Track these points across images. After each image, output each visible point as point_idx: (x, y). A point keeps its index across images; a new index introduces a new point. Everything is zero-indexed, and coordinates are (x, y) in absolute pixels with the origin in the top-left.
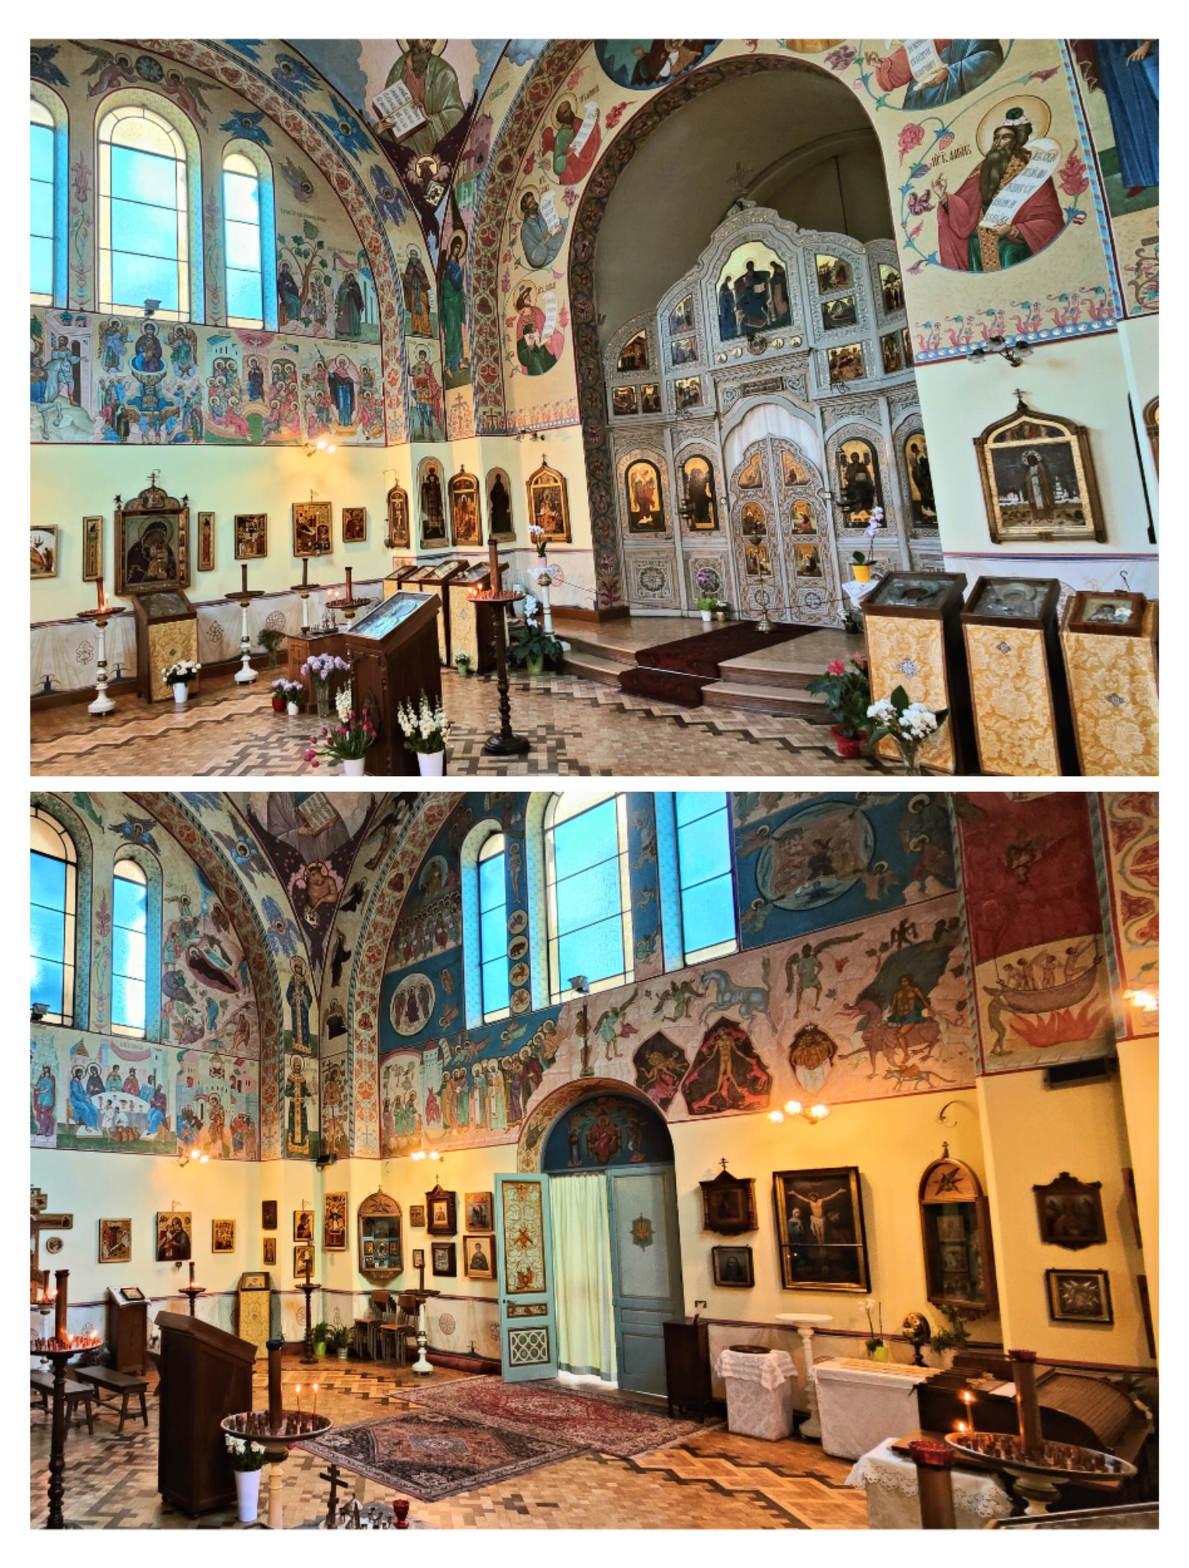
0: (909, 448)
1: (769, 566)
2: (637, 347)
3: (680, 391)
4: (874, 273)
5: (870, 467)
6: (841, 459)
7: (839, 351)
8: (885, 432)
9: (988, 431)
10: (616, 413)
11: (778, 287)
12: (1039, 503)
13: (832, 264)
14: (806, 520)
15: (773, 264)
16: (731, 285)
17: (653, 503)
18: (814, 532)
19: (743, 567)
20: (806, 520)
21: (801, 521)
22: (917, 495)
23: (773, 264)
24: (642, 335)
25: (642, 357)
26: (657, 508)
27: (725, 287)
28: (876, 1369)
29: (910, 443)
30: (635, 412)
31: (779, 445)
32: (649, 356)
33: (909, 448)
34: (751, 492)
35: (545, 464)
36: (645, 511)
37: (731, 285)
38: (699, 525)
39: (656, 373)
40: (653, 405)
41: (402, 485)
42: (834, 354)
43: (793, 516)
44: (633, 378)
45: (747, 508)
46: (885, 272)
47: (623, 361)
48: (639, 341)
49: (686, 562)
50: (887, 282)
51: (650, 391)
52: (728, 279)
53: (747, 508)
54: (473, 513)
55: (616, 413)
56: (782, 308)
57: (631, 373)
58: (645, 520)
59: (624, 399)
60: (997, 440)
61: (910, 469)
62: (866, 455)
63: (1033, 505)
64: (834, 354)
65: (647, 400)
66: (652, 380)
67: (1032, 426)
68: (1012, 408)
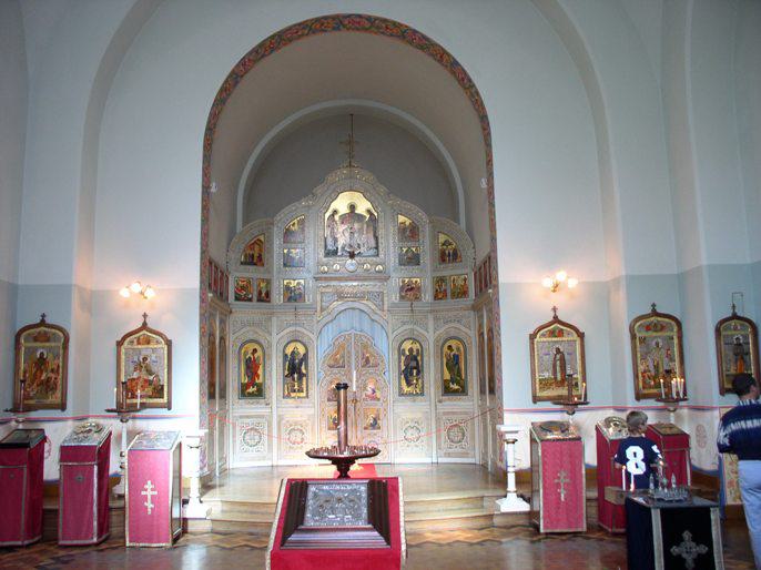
0: (446, 346)
3: (287, 288)
4: (435, 238)
5: (419, 358)
6: (401, 352)
7: (407, 280)
10: (237, 299)
12: (559, 377)
13: (407, 223)
14: (374, 392)
15: (369, 211)
18: (379, 399)
20: (374, 392)
22: (447, 376)
23: (369, 211)
25: (260, 257)
28: (719, 557)
29: (448, 344)
30: (250, 300)
32: (265, 256)
33: (446, 346)
34: (336, 370)
35: (145, 324)
36: (252, 383)
38: (293, 395)
39: (269, 271)
40: (265, 297)
42: (403, 282)
43: (365, 389)
44: (252, 273)
46: (442, 238)
47: (246, 256)
50: (443, 245)
51: (263, 285)
52: (335, 212)
55: (237, 299)
57: (252, 268)
58: (251, 390)
59: (243, 288)
60: (543, 335)
62: (418, 350)
63: (556, 378)
64: (403, 282)
65: (260, 293)
66: (266, 276)
67: (46, 333)
68: (551, 319)
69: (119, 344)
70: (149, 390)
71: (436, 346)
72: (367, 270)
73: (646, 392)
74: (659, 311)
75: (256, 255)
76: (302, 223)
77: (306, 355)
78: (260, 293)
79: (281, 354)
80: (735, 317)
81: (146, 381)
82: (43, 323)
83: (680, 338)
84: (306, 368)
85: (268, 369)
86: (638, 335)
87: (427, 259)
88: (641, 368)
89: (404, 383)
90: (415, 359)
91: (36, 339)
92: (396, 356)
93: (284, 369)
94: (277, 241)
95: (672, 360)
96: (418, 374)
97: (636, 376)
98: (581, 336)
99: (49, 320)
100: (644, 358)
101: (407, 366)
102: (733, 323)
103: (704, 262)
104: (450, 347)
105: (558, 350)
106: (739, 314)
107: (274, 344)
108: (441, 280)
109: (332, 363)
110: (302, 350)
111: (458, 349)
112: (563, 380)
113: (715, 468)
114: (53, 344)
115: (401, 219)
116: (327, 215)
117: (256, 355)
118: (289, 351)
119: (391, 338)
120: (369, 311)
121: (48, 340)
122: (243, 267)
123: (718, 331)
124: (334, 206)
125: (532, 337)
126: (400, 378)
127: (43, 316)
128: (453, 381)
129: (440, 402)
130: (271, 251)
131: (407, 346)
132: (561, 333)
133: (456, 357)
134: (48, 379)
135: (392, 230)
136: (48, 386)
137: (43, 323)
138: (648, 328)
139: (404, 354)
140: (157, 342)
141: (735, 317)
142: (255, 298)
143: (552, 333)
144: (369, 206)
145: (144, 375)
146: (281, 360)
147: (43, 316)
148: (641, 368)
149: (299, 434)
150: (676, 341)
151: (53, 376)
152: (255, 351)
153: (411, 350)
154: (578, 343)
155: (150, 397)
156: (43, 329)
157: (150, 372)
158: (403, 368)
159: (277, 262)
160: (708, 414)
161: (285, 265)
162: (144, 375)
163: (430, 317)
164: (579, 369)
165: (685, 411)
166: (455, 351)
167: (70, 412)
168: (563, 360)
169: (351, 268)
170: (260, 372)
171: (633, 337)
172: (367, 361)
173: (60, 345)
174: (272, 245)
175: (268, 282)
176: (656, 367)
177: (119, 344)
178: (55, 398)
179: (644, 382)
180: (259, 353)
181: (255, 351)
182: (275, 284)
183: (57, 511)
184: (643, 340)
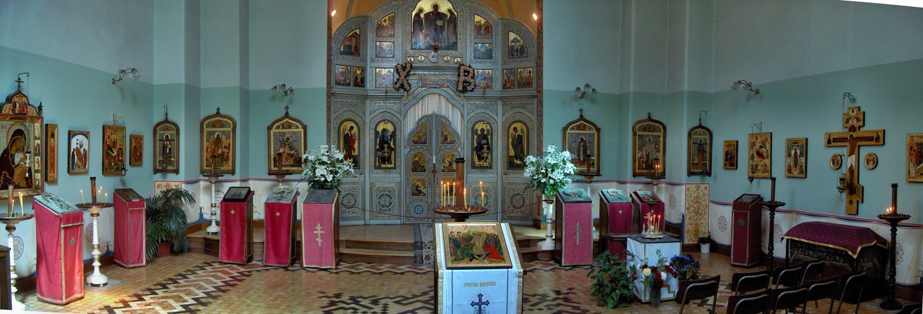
0: (511, 130)
1: (424, 191)
2: (354, 39)
6: (474, 131)
8: (500, 120)
9: (273, 124)
11: (451, 26)
15: (450, 11)
16: (422, 16)
17: (354, 150)
19: (409, 191)
21: (447, 164)
22: (512, 153)
24: (358, 31)
26: (356, 153)
27: (418, 15)
30: (348, 85)
31: (441, 121)
33: (511, 130)
35: (287, 113)
37: (422, 16)
38: (383, 166)
39: (365, 61)
41: (171, 118)
43: (444, 161)
45: (415, 156)
48: (355, 35)
49: (371, 189)
51: (358, 72)
52: (421, 11)
53: (415, 156)
54: (228, 147)
56: (452, 40)
57: (349, 57)
60: (572, 129)
61: (510, 140)
65: (356, 78)
67: (220, 121)
68: (578, 117)
69: (270, 128)
70: (291, 161)
71: (503, 126)
72: (447, 62)
73: (641, 171)
74: (654, 117)
75: (353, 45)
76: (392, 20)
77: (394, 133)
78: (356, 78)
79: (373, 132)
80: (700, 126)
81: (289, 154)
82: (218, 114)
83: (665, 137)
84: (394, 144)
85: (362, 144)
86: (638, 133)
87: (498, 55)
88: (638, 156)
89: (476, 158)
90: (485, 137)
91: (214, 126)
92: (470, 136)
93: (376, 144)
94: (371, 36)
95: (658, 151)
96: (488, 149)
97: (634, 161)
98: (598, 130)
99: (222, 112)
100: (640, 149)
101: (479, 143)
102: (699, 130)
103: (686, 88)
104: (515, 129)
105: (582, 139)
106: (703, 125)
107: (368, 122)
108: (512, 71)
109: (416, 139)
110: (390, 128)
111: (522, 130)
112: (584, 161)
113: (680, 221)
114: (225, 129)
115: (477, 18)
116: (414, 13)
117: (353, 132)
118: (380, 129)
119: (466, 120)
120: (448, 97)
121: (222, 127)
122: (341, 56)
123: (690, 135)
124: (419, 5)
125: (565, 129)
126: (472, 154)
127: (218, 109)
128: (516, 157)
129: (505, 174)
130: (366, 44)
131: (479, 127)
132: (584, 128)
133: (520, 138)
134: (223, 153)
135: (470, 28)
136: (224, 158)
137: (218, 114)
138: (644, 129)
139: (476, 133)
140: (297, 127)
141: (700, 126)
142: (352, 83)
143: (579, 128)
144: (450, 6)
145: (287, 150)
146: (373, 137)
147: (218, 109)
148: (638, 156)
149: (388, 199)
150: (662, 139)
151: (226, 151)
152: (352, 128)
153: (482, 130)
154: (60, 302)
155: (292, 166)
156: (218, 118)
157: (291, 148)
158: (475, 145)
159: (370, 52)
160: (677, 188)
161: (377, 56)
162: (287, 150)
163: (500, 103)
164: (596, 152)
165: (664, 185)
166: (519, 133)
167: (237, 175)
168: (585, 147)
169: (433, 60)
170: (356, 146)
171: (635, 134)
172: (446, 138)
173: (230, 129)
174: (366, 38)
175: (363, 70)
176: (648, 156)
177: (270, 128)
178: (227, 167)
179: (639, 165)
180: (355, 130)
181: (352, 128)
182: (369, 70)
183: (218, 241)
184: (641, 137)
